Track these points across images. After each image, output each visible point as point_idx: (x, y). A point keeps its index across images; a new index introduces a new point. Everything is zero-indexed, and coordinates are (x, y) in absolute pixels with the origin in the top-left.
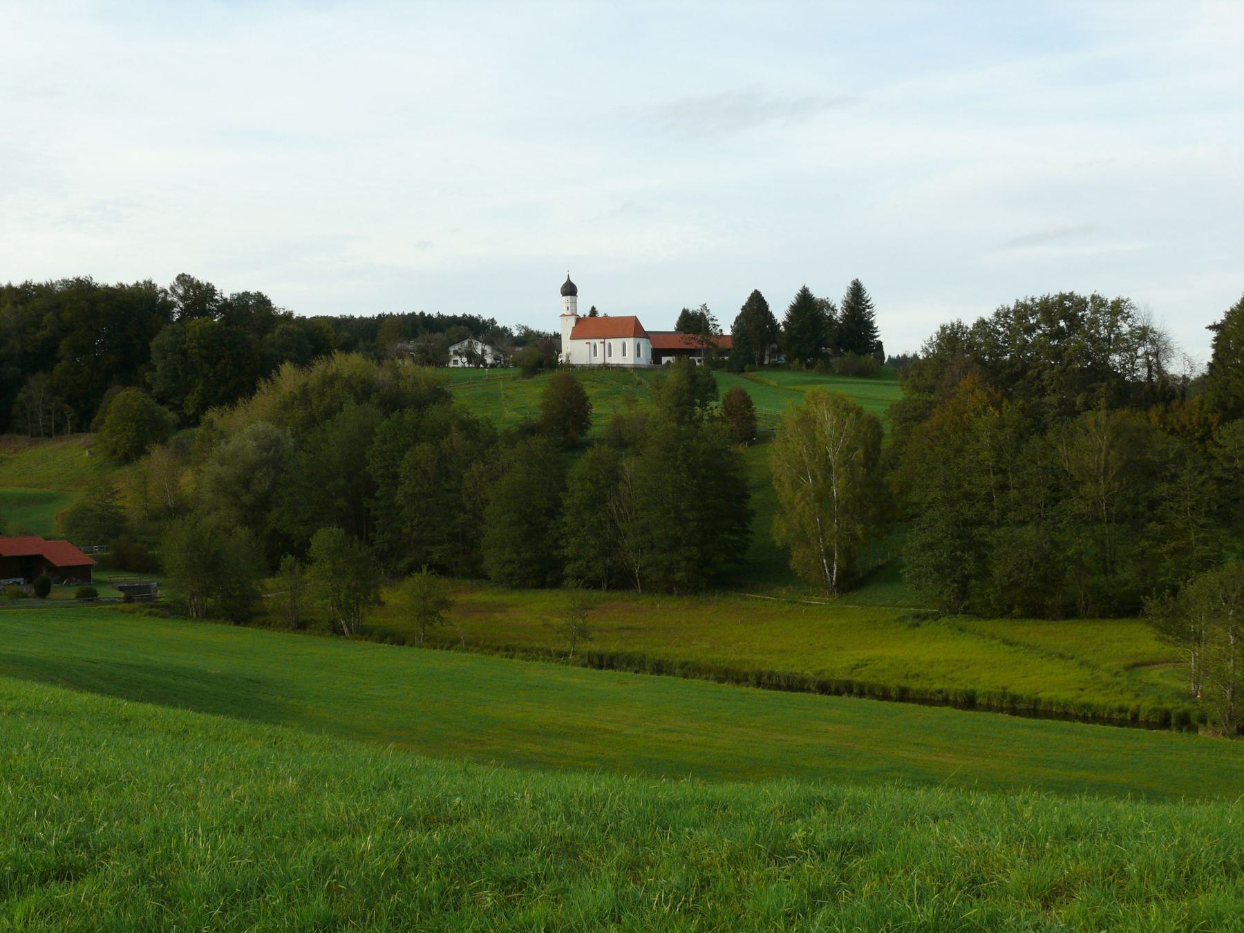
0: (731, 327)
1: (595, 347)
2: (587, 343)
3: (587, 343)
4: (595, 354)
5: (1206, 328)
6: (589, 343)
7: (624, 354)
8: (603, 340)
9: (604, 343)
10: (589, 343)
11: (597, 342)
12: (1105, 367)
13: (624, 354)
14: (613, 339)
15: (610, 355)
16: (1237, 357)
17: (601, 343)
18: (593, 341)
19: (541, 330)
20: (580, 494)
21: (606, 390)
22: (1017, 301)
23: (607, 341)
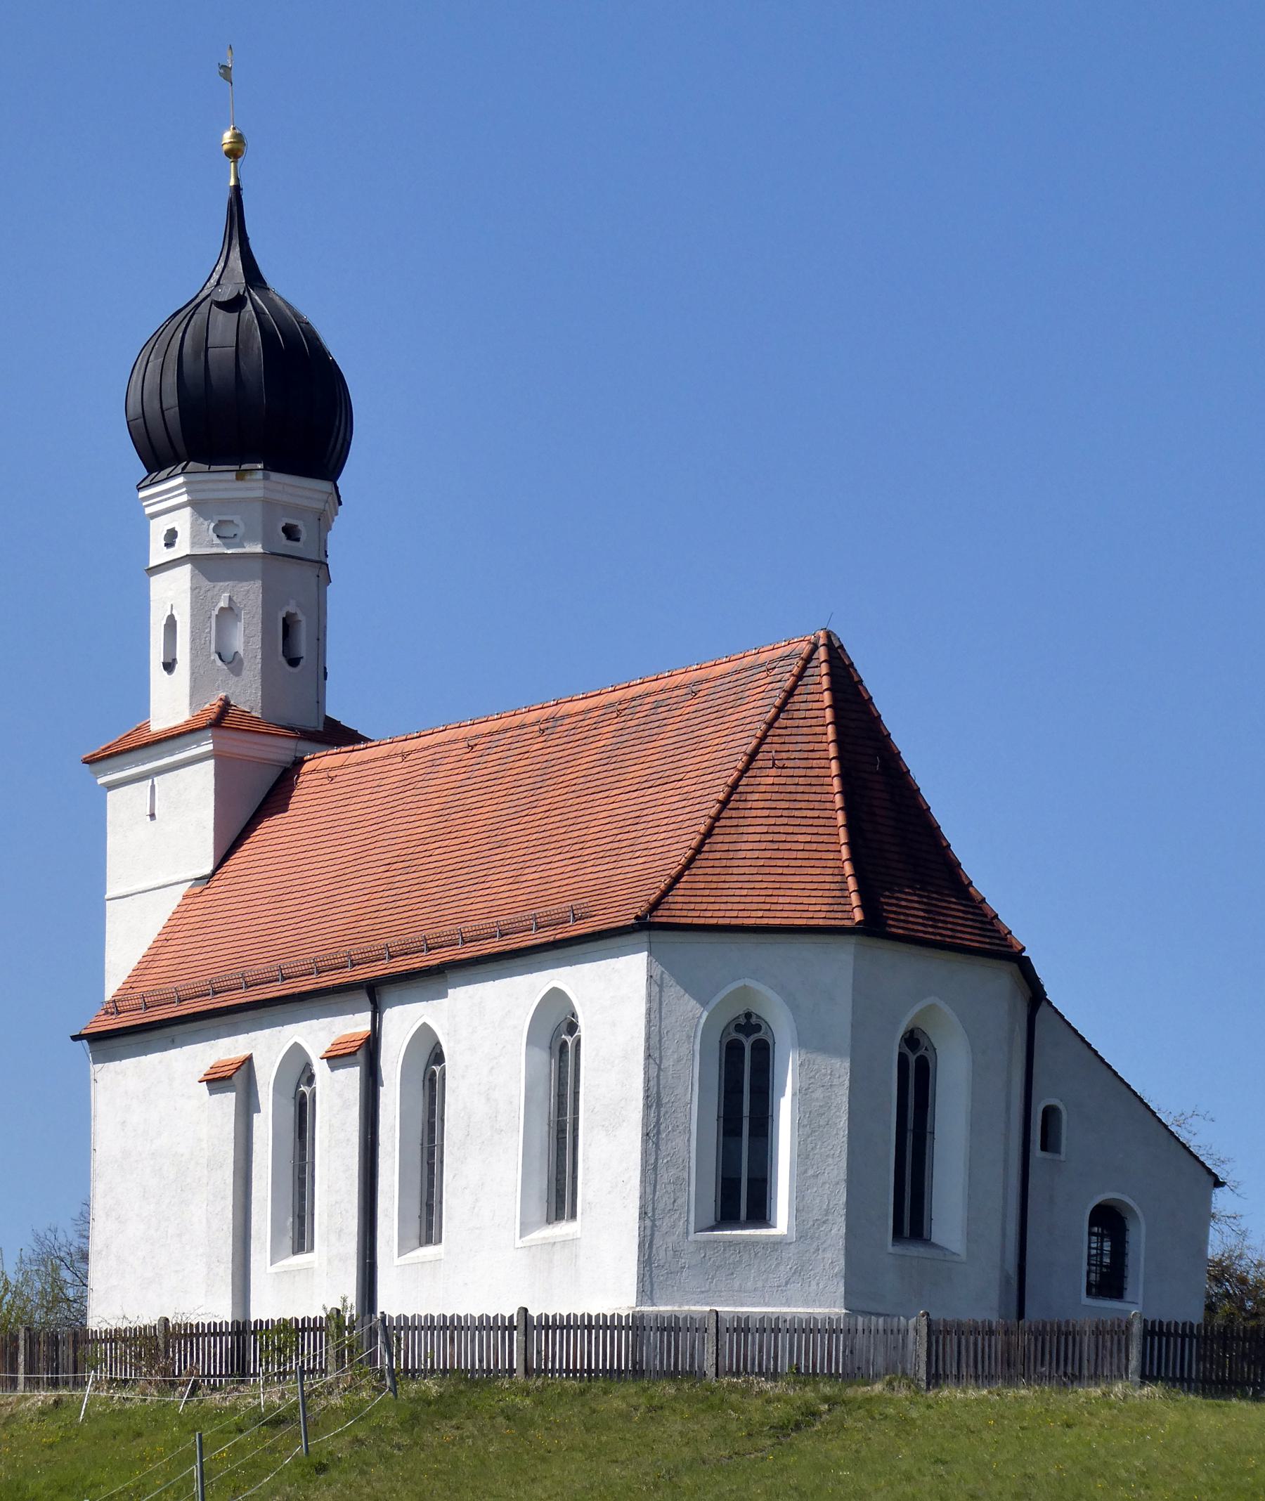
8: (357, 1024)
9: (371, 1047)
17: (336, 1059)
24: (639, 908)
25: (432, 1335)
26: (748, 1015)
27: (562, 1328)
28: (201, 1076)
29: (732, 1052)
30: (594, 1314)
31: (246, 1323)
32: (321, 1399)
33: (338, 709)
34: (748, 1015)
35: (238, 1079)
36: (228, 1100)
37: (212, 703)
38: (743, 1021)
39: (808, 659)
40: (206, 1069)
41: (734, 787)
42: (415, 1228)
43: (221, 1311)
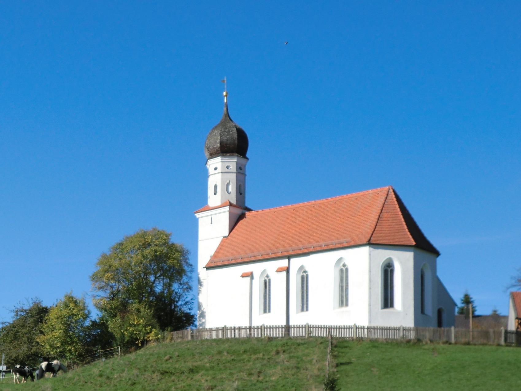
0: (211, 256)
1: (267, 285)
2: (244, 276)
3: (244, 276)
4: (267, 308)
5: (204, 268)
6: (250, 275)
7: (343, 301)
8: (284, 263)
9: (288, 270)
10: (250, 275)
11: (271, 267)
12: (88, 342)
13: (343, 301)
14: (313, 257)
15: (304, 306)
16: (91, 341)
17: (279, 270)
18: (256, 268)
19: (207, 262)
20: (22, 313)
21: (38, 316)
22: (89, 276)
23: (296, 263)
24: (367, 240)
25: (275, 329)
26: (389, 264)
27: (301, 327)
28: (276, 271)
29: (303, 277)
30: (329, 325)
31: (251, 327)
32: (71, 322)
33: (248, 205)
34: (389, 264)
35: (250, 276)
36: (284, 274)
37: (226, 200)
38: (388, 265)
39: (388, 192)
40: (241, 274)
41: (379, 216)
42: (300, 308)
43: (247, 325)
